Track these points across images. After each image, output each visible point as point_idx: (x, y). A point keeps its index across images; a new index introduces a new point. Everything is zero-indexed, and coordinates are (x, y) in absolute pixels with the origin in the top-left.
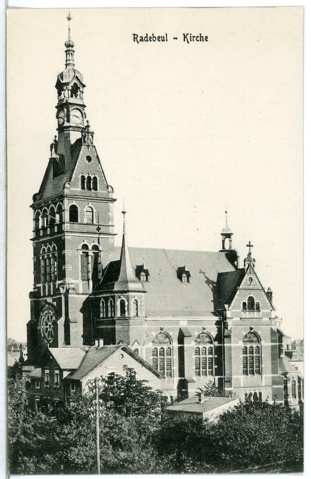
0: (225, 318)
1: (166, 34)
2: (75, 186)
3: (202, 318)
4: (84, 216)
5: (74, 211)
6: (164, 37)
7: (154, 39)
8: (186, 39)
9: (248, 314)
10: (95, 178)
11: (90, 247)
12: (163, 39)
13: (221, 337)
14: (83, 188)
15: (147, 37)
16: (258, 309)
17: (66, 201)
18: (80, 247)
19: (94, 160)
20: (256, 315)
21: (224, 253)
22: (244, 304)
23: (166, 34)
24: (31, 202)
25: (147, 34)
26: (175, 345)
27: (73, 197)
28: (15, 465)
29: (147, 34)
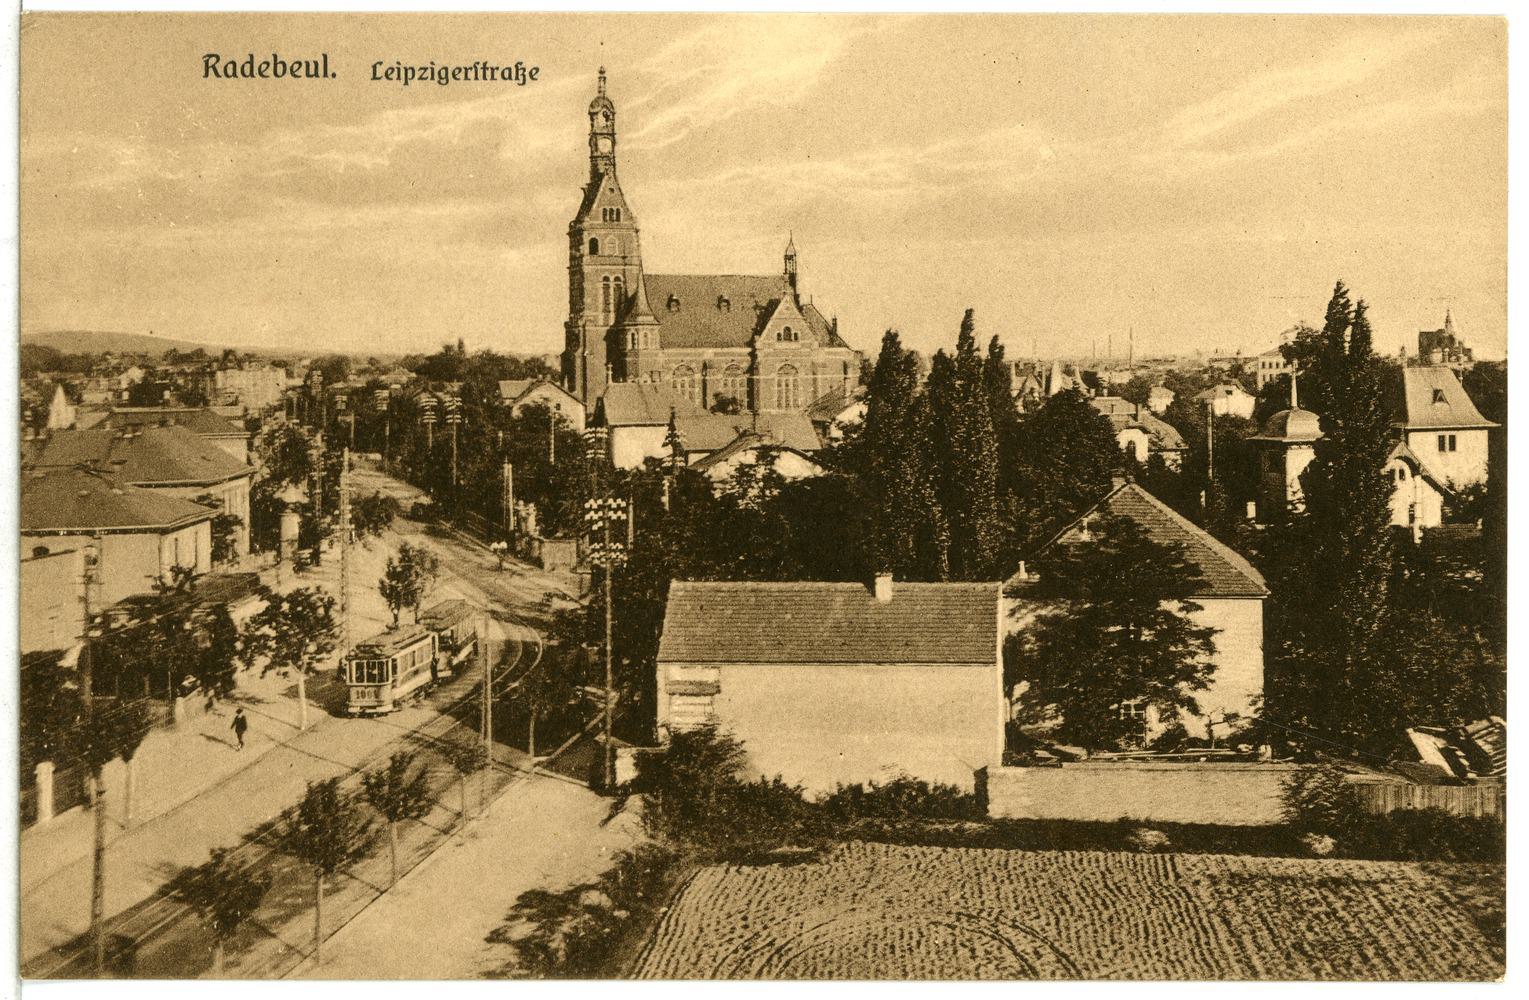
0: (755, 350)
1: (325, 56)
2: (597, 218)
3: (734, 350)
4: (605, 248)
5: (594, 244)
6: (316, 63)
7: (280, 68)
8: (211, 71)
9: (784, 345)
10: (618, 210)
11: (612, 278)
12: (312, 72)
13: (752, 369)
14: (605, 220)
15: (251, 63)
16: (796, 338)
17: (585, 233)
18: (601, 279)
19: (616, 192)
20: (793, 345)
21: (611, 423)
22: (779, 335)
23: (325, 56)
24: (568, 230)
25: (252, 56)
26: (698, 376)
27: (592, 228)
28: (28, 968)
29: (252, 56)
